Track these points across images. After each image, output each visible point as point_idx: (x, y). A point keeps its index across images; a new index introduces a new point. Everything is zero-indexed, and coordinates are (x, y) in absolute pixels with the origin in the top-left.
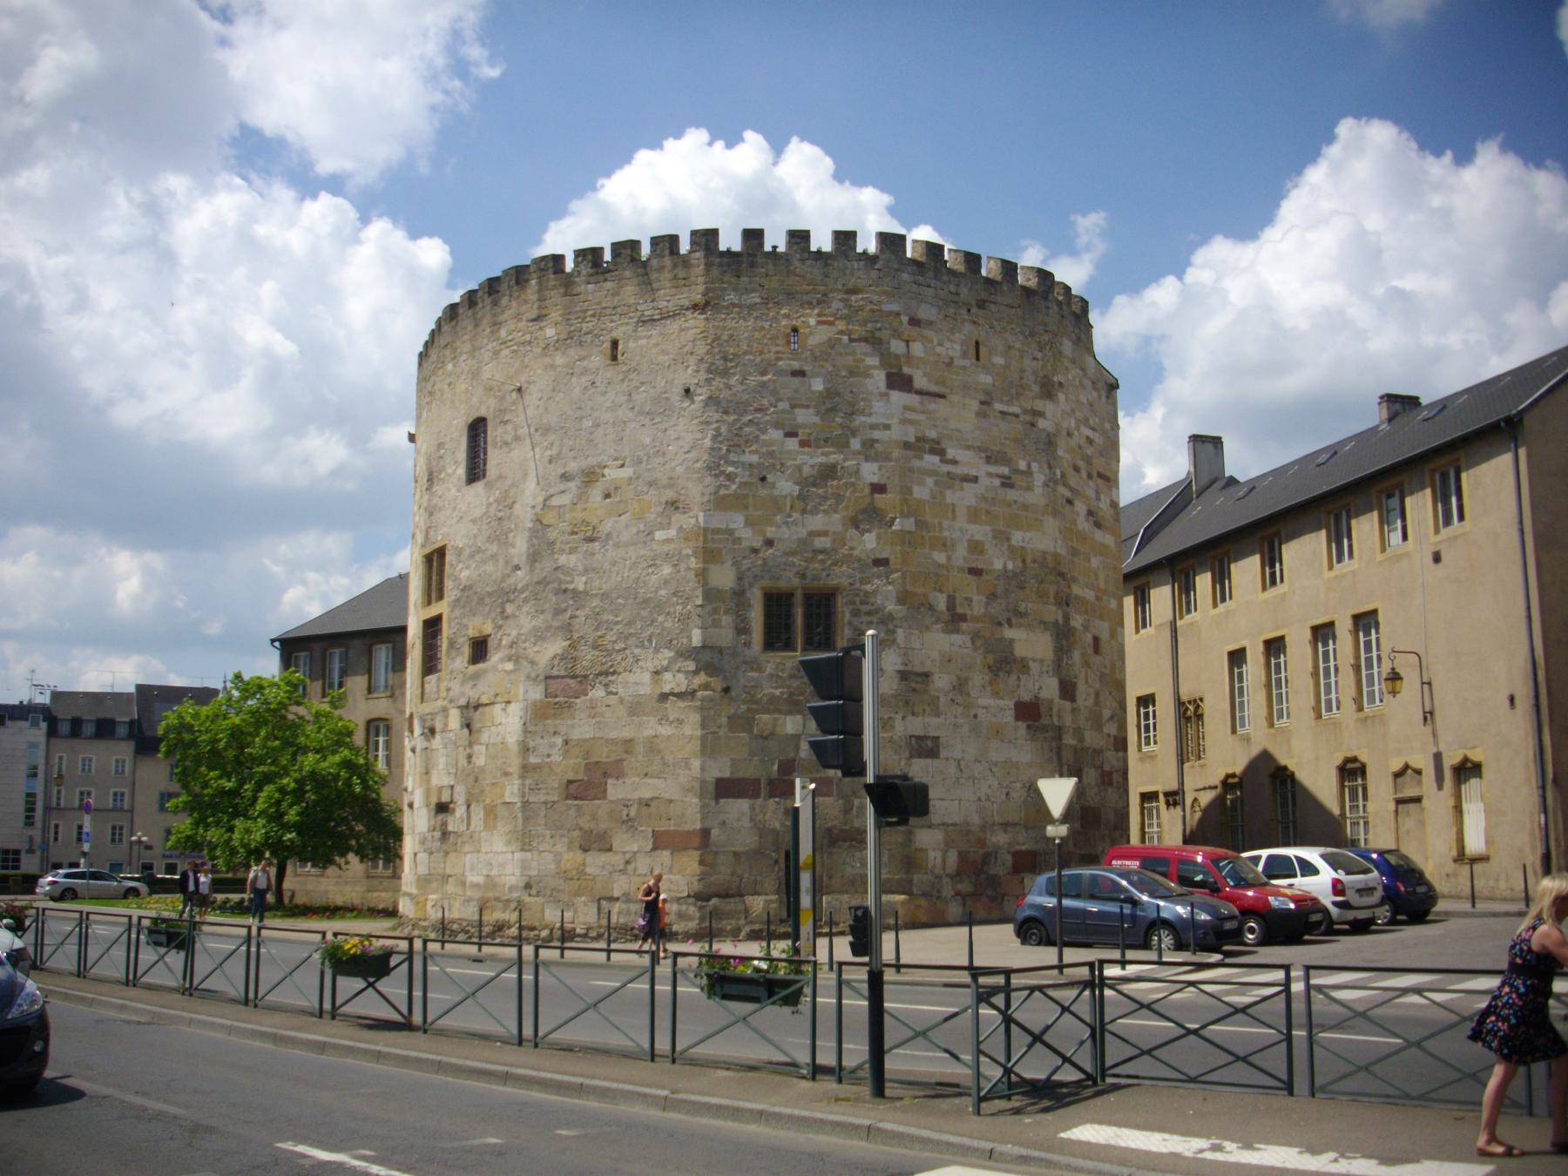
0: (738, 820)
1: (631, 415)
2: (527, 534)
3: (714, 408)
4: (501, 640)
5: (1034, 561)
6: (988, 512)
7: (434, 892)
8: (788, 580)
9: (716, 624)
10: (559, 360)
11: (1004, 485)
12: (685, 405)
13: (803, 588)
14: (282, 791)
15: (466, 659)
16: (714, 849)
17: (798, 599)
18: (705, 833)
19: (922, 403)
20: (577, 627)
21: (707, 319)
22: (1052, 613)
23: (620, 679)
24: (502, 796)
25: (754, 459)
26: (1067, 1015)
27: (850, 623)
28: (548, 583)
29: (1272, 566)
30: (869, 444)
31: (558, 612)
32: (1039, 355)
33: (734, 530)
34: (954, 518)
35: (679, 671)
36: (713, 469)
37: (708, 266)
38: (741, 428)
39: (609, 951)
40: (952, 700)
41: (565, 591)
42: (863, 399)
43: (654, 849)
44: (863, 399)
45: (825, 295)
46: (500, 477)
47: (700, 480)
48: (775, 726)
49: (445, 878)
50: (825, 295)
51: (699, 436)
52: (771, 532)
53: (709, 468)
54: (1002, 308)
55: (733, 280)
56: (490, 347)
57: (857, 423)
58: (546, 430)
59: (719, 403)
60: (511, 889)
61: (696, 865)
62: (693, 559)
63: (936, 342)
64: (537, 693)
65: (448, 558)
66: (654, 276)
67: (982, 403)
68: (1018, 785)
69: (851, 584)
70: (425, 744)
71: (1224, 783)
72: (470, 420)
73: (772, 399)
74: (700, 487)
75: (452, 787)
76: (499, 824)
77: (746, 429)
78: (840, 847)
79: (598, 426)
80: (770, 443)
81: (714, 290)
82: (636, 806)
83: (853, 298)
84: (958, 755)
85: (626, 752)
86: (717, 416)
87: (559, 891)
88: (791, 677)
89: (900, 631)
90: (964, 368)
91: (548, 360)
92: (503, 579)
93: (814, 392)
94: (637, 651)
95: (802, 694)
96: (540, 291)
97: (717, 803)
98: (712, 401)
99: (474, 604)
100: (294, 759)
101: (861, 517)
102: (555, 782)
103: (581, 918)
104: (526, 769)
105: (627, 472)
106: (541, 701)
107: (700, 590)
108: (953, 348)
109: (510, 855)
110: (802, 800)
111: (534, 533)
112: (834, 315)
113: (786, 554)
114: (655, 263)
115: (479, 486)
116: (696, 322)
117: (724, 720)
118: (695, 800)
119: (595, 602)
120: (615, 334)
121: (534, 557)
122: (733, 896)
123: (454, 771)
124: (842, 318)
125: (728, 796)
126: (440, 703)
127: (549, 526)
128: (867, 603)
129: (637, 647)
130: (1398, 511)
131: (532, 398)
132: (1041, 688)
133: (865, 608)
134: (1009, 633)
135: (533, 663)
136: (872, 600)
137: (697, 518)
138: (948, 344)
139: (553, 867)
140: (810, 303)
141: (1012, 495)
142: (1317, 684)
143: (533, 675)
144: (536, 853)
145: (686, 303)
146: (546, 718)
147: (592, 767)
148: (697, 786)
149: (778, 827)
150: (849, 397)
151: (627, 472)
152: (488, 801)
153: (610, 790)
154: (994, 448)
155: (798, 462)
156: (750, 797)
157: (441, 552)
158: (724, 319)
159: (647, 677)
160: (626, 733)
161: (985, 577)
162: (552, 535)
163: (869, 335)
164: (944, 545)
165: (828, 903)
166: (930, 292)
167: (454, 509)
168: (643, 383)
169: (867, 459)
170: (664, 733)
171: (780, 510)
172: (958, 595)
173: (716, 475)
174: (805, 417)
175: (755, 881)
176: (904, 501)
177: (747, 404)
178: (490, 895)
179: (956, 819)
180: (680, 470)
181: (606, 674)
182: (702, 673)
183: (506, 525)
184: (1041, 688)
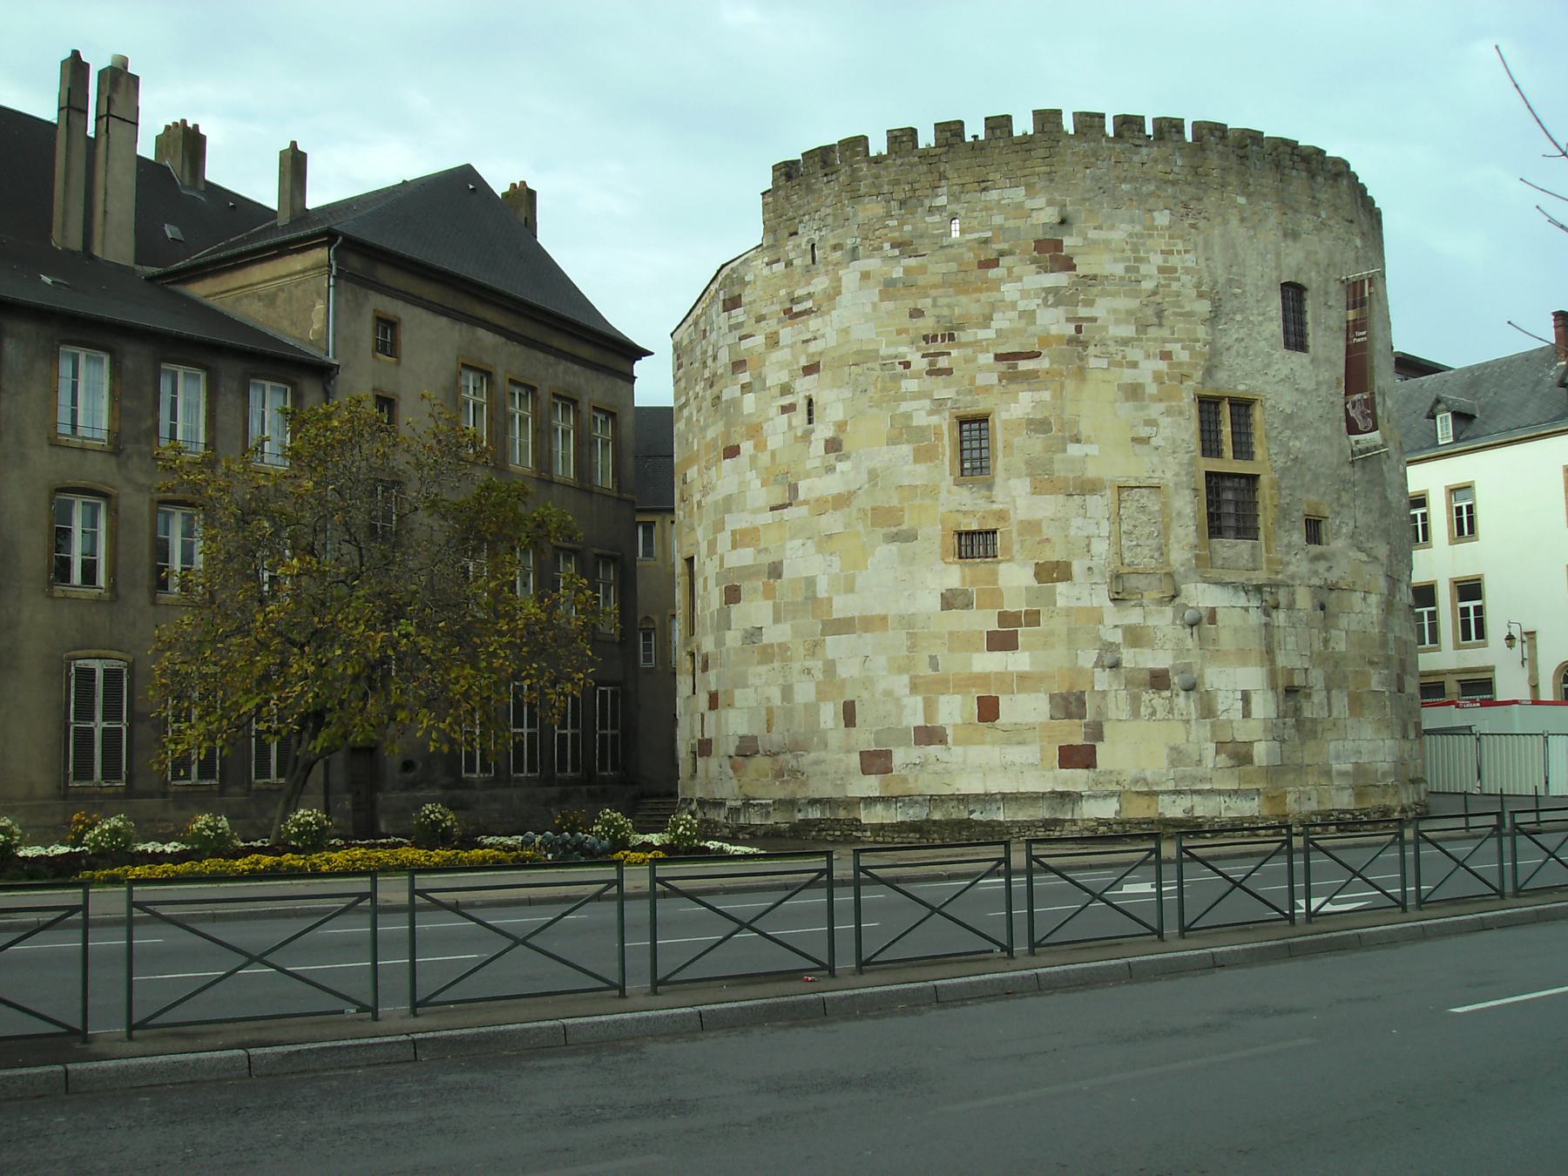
24: (1369, 684)
26: (1237, 877)
49: (1300, 769)
60: (1384, 775)
76: (1366, 712)
152: (1352, 688)
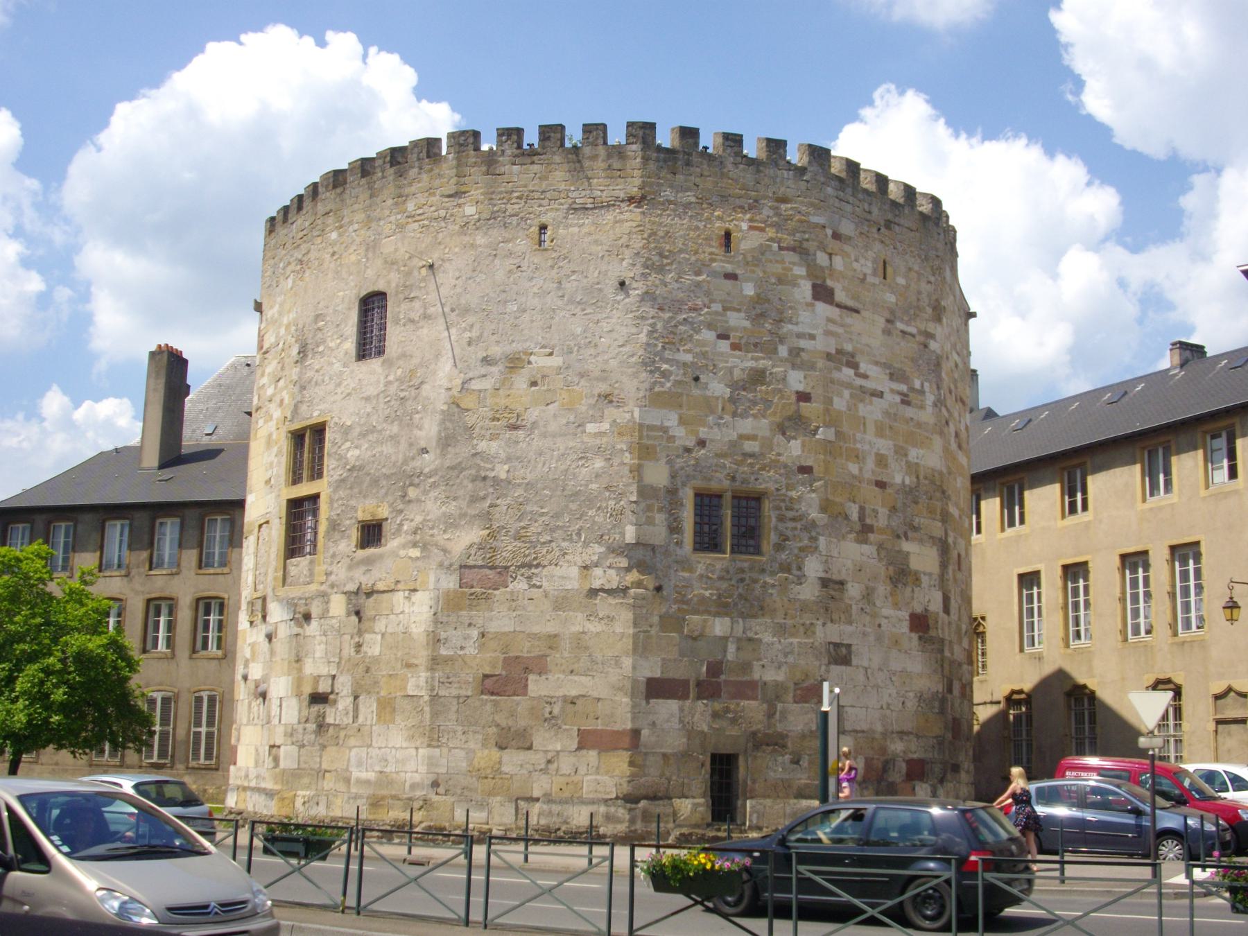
0: (668, 721)
1: (560, 303)
2: (438, 417)
3: (649, 304)
4: (401, 525)
5: (926, 478)
6: (891, 427)
7: (308, 788)
8: (720, 482)
9: (650, 521)
10: (480, 240)
11: (903, 402)
12: (619, 298)
13: (733, 491)
14: (47, 671)
15: (354, 543)
16: (644, 750)
17: (727, 499)
18: (636, 733)
19: (841, 316)
20: (497, 516)
21: (643, 213)
22: (937, 529)
23: (545, 572)
24: (405, 688)
25: (688, 358)
27: (776, 528)
28: (463, 469)
29: (1072, 494)
30: (795, 352)
31: (474, 499)
32: (932, 279)
33: (667, 427)
34: (865, 432)
35: (609, 567)
36: (649, 364)
37: (646, 159)
38: (676, 326)
39: (1062, 863)
40: (862, 609)
41: (485, 478)
42: (791, 308)
43: (580, 748)
44: (791, 308)
45: (756, 201)
46: (404, 355)
47: (635, 375)
48: (704, 627)
49: (321, 773)
50: (756, 201)
51: (634, 330)
52: (703, 432)
53: (644, 364)
54: (905, 230)
55: (669, 176)
56: (392, 218)
57: (785, 330)
58: (466, 311)
59: (655, 299)
60: (414, 786)
61: (626, 765)
62: (627, 454)
63: (853, 258)
64: (450, 582)
65: (329, 435)
66: (587, 164)
67: (888, 321)
68: (911, 695)
69: (778, 490)
71: (1009, 699)
72: (363, 293)
73: (706, 300)
74: (635, 382)
75: (334, 677)
77: (680, 327)
78: (764, 752)
79: (525, 311)
80: (703, 343)
81: (651, 185)
82: (560, 703)
83: (783, 207)
84: (865, 664)
85: (550, 648)
86: (652, 312)
87: (471, 790)
88: (721, 578)
89: (822, 539)
90: (874, 285)
91: (466, 239)
92: (405, 462)
93: (746, 296)
94: (564, 544)
95: (731, 596)
96: (459, 166)
97: (648, 703)
98: (648, 296)
99: (365, 485)
100: (55, 640)
101: (787, 424)
102: (469, 676)
103: (497, 819)
104: (435, 662)
105: (556, 361)
106: (455, 591)
107: (636, 485)
108: (866, 266)
109: (413, 752)
110: (830, 704)
111: (447, 417)
112: (765, 222)
114: (587, 151)
115: (375, 364)
116: (632, 215)
117: (656, 619)
118: (626, 700)
119: (519, 492)
120: (544, 220)
121: (446, 441)
122: (661, 798)
123: (337, 660)
124: (772, 225)
125: (658, 696)
126: (314, 587)
127: (467, 410)
128: (792, 509)
129: (564, 540)
130: (1225, 451)
131: (447, 277)
132: (929, 601)
133: (790, 514)
134: (907, 546)
135: (445, 551)
136: (796, 507)
137: (632, 413)
138: (862, 261)
139: (464, 764)
140: (742, 207)
141: (909, 412)
142: (1124, 609)
143: (446, 563)
144: (445, 750)
145: (622, 195)
147: (510, 662)
148: (628, 685)
149: (706, 728)
151: (556, 361)
152: (383, 693)
154: (896, 365)
155: (729, 365)
156: (679, 698)
157: (319, 431)
158: (661, 215)
159: (574, 572)
160: (551, 628)
161: (889, 490)
162: (470, 419)
163: (797, 244)
164: (857, 457)
165: (752, 807)
166: (849, 208)
167: (339, 385)
168: (574, 272)
169: (794, 367)
171: (712, 411)
172: (867, 506)
173: (651, 372)
174: (737, 320)
175: (683, 783)
176: (827, 411)
177: (682, 302)
178: (384, 792)
179: (865, 727)
180: (613, 363)
181: (530, 566)
182: (635, 570)
183: (410, 405)
184: (929, 601)
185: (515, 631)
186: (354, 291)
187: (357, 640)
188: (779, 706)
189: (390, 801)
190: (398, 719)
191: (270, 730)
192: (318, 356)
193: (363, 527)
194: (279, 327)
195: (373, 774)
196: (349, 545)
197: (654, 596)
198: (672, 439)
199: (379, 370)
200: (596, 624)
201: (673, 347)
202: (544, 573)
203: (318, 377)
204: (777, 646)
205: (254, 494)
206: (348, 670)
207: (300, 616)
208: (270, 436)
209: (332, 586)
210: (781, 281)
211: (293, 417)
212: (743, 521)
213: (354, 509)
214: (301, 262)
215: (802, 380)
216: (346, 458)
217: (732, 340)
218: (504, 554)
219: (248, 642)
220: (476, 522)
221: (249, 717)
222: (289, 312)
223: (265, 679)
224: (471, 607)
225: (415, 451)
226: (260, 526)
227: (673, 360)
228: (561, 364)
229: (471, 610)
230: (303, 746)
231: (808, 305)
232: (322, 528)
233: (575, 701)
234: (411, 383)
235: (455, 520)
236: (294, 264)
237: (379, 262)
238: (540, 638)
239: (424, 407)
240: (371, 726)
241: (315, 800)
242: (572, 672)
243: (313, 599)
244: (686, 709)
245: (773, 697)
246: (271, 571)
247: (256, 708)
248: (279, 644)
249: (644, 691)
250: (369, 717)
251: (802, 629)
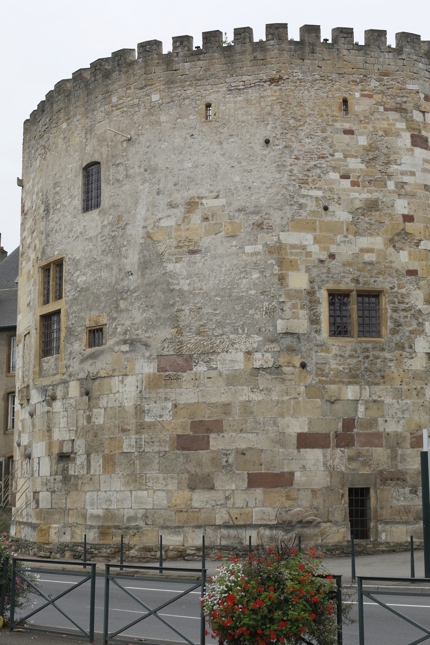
1: (223, 159)
12: (265, 152)
20: (183, 318)
24: (122, 447)
25: (319, 193)
49: (65, 511)
51: (278, 176)
52: (333, 249)
55: (299, 61)
62: (276, 267)
65: (65, 267)
69: (392, 288)
70: (47, 408)
72: (85, 164)
75: (74, 440)
78: (389, 485)
82: (233, 454)
85: (225, 413)
92: (117, 283)
94: (232, 336)
97: (299, 452)
101: (396, 238)
102: (165, 436)
106: (154, 374)
109: (129, 494)
111: (144, 247)
113: (344, 265)
115: (94, 213)
120: (208, 100)
123: (75, 429)
126: (58, 377)
133: (403, 306)
136: (406, 301)
139: (165, 502)
144: (151, 492)
145: (265, 78)
146: (159, 388)
147: (196, 425)
150: (385, 151)
152: (106, 452)
153: (212, 442)
159: (240, 356)
160: (224, 399)
162: (161, 248)
167: (71, 231)
170: (256, 398)
178: (110, 524)
185: (198, 402)
186: (79, 164)
187: (88, 413)
188: (400, 452)
189: (114, 530)
190: (118, 470)
191: (33, 481)
192: (57, 212)
193: (90, 331)
194: (33, 195)
195: (102, 510)
196: (80, 345)
197: (301, 372)
198: (309, 254)
199: (97, 218)
200: (258, 394)
201: (307, 186)
202: (218, 358)
203: (57, 227)
204: (396, 406)
205: (21, 314)
206: (83, 435)
207: (49, 398)
208: (29, 272)
209: (70, 376)
210: (386, 133)
211: (42, 257)
212: (366, 313)
213: (83, 319)
214: (44, 147)
215: (407, 206)
216: (77, 283)
217: (351, 179)
218: (189, 345)
219: (20, 419)
220: (168, 323)
221: (22, 472)
222: (38, 183)
223: (30, 445)
224: (166, 386)
225: (123, 274)
226: (25, 336)
227: (307, 196)
228: (225, 204)
229: (167, 388)
230: (54, 492)
231: (408, 150)
232: (63, 334)
233: (244, 452)
234: (119, 226)
235: (153, 323)
236: (40, 149)
237: (94, 142)
238: (217, 406)
239: (128, 242)
240: (99, 475)
241: (63, 531)
242: (241, 430)
243: (57, 385)
244: (328, 455)
245: (395, 444)
246: (31, 367)
247: (25, 466)
248: (37, 419)
249: (295, 442)
250: (98, 469)
251: (414, 393)
